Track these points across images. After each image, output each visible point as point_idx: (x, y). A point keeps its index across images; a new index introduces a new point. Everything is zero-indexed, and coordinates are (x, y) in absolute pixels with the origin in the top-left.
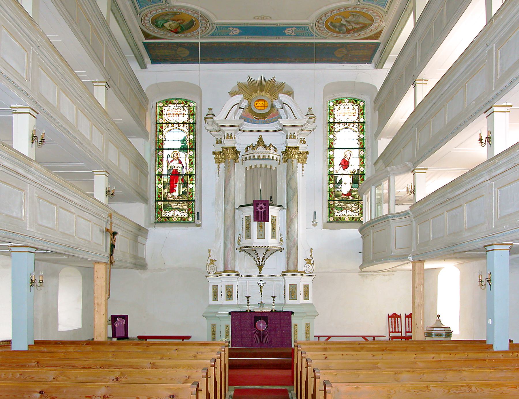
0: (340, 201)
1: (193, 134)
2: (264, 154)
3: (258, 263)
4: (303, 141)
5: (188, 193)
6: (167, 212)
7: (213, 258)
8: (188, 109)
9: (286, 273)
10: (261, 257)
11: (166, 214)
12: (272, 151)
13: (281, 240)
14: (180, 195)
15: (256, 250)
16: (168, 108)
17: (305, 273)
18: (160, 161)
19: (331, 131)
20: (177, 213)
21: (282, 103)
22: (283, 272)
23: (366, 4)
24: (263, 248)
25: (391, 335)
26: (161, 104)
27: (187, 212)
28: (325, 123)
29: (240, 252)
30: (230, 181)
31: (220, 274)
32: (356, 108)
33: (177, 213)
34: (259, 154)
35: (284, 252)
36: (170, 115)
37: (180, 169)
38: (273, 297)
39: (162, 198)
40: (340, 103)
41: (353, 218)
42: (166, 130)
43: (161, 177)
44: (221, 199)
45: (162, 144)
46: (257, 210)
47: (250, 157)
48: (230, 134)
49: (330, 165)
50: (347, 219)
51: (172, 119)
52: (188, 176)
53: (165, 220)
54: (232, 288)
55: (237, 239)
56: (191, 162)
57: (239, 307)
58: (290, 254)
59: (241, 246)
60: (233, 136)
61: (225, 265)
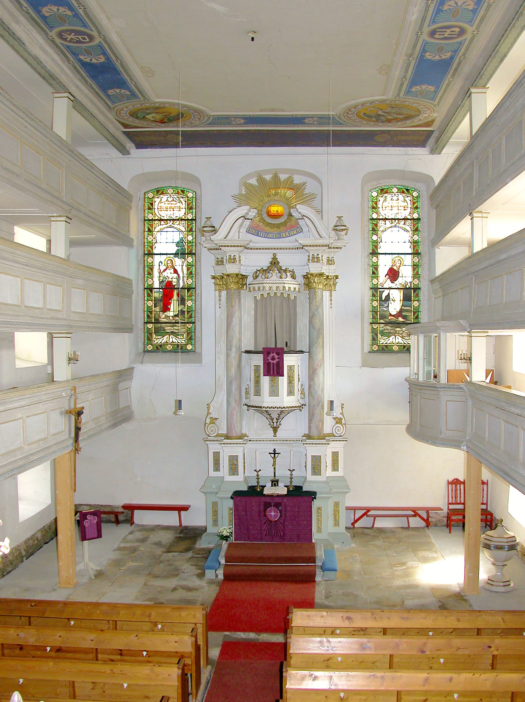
0: (386, 324)
1: (192, 234)
3: (272, 424)
4: (330, 262)
5: (186, 312)
6: (159, 337)
7: (214, 416)
8: (185, 202)
14: (176, 316)
16: (159, 199)
17: (334, 436)
18: (150, 271)
19: (374, 230)
23: (409, 99)
24: (277, 409)
25: (452, 507)
26: (151, 195)
28: (366, 219)
32: (408, 199)
34: (271, 285)
35: (306, 409)
37: (175, 280)
40: (386, 193)
41: (404, 346)
42: (157, 230)
43: (152, 292)
44: (223, 338)
46: (268, 361)
47: (259, 288)
50: (395, 348)
51: (165, 215)
52: (186, 290)
53: (157, 348)
54: (237, 459)
55: (243, 394)
56: (190, 271)
60: (237, 259)
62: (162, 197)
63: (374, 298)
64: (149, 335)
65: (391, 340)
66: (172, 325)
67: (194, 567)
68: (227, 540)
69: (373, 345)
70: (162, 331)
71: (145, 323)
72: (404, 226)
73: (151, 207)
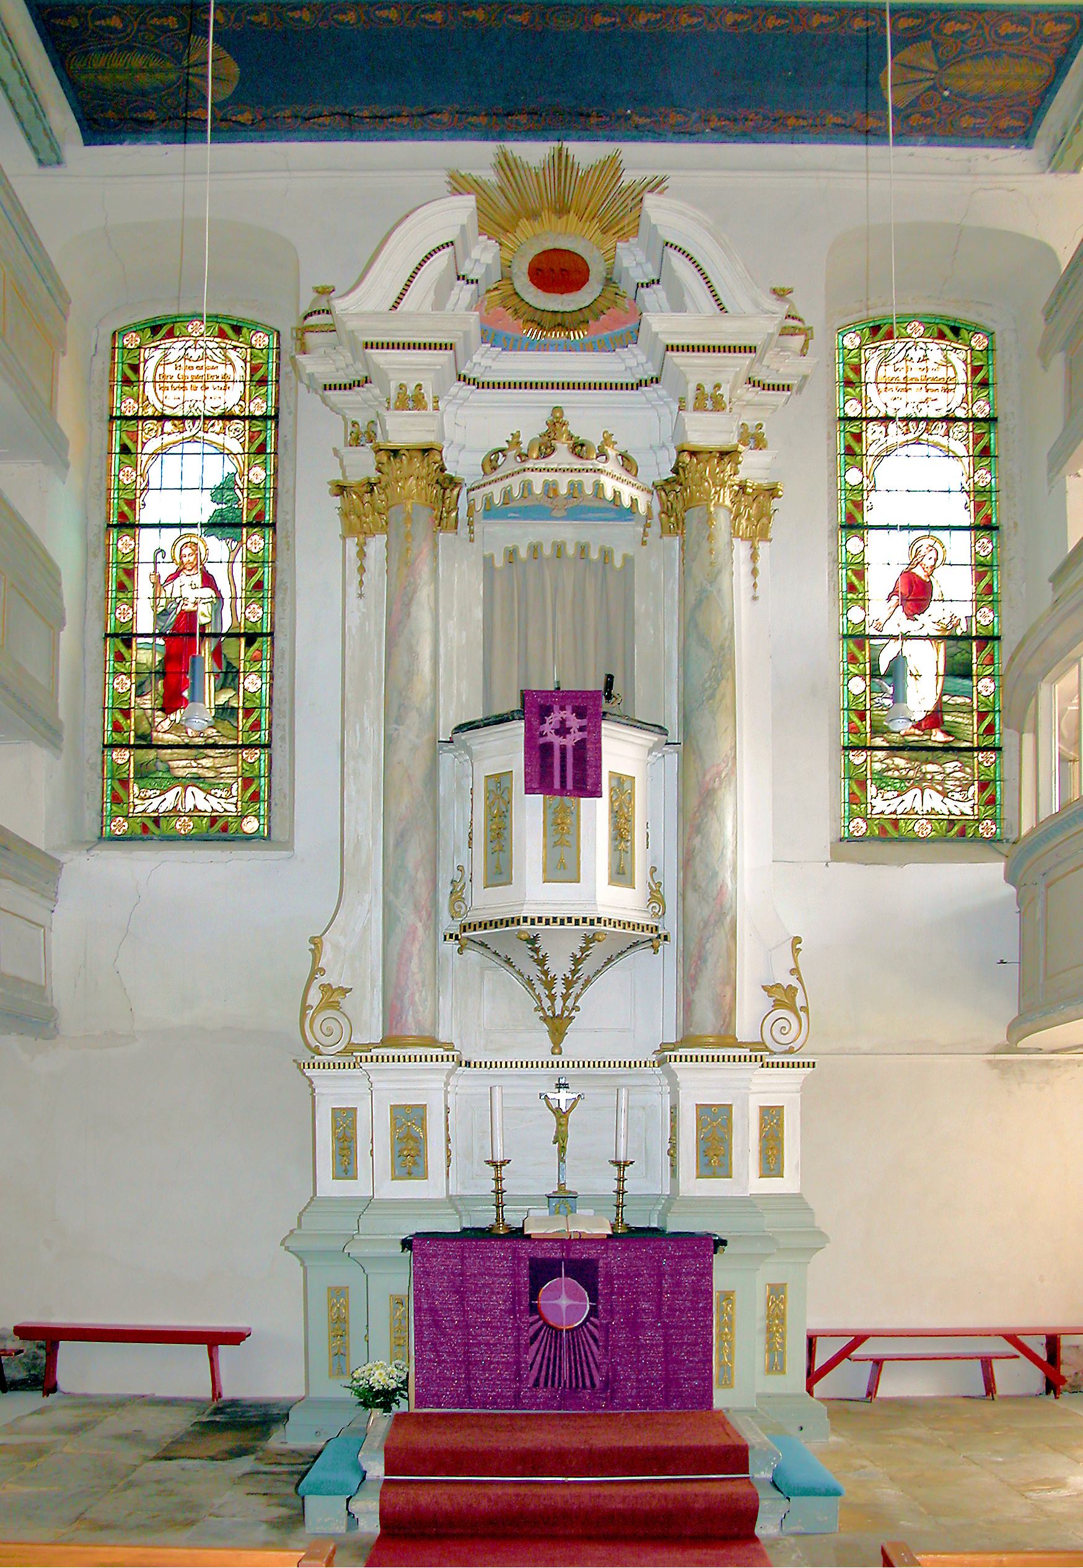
0: (893, 749)
1: (265, 462)
2: (575, 477)
3: (546, 1003)
5: (241, 711)
6: (150, 793)
7: (331, 978)
8: (245, 361)
9: (683, 1052)
10: (560, 976)
11: (148, 802)
12: (612, 466)
13: (656, 896)
15: (536, 938)
16: (158, 354)
20: (196, 799)
21: (660, 245)
22: (664, 1047)
27: (234, 793)
29: (460, 951)
30: (414, 608)
31: (364, 1054)
33: (196, 799)
34: (550, 477)
36: (169, 385)
38: (617, 1163)
39: (132, 733)
41: (952, 823)
45: (131, 504)
46: (541, 741)
48: (411, 387)
49: (850, 596)
50: (923, 829)
51: (172, 401)
52: (243, 640)
55: (445, 890)
56: (255, 579)
57: (458, 1212)
58: (701, 958)
59: (468, 920)
61: (392, 1012)
62: (168, 346)
63: (853, 669)
64: (117, 786)
65: (907, 805)
66: (194, 752)
67: (263, 1499)
68: (386, 1407)
69: (851, 818)
70: (160, 774)
71: (105, 746)
72: (944, 441)
73: (133, 377)
